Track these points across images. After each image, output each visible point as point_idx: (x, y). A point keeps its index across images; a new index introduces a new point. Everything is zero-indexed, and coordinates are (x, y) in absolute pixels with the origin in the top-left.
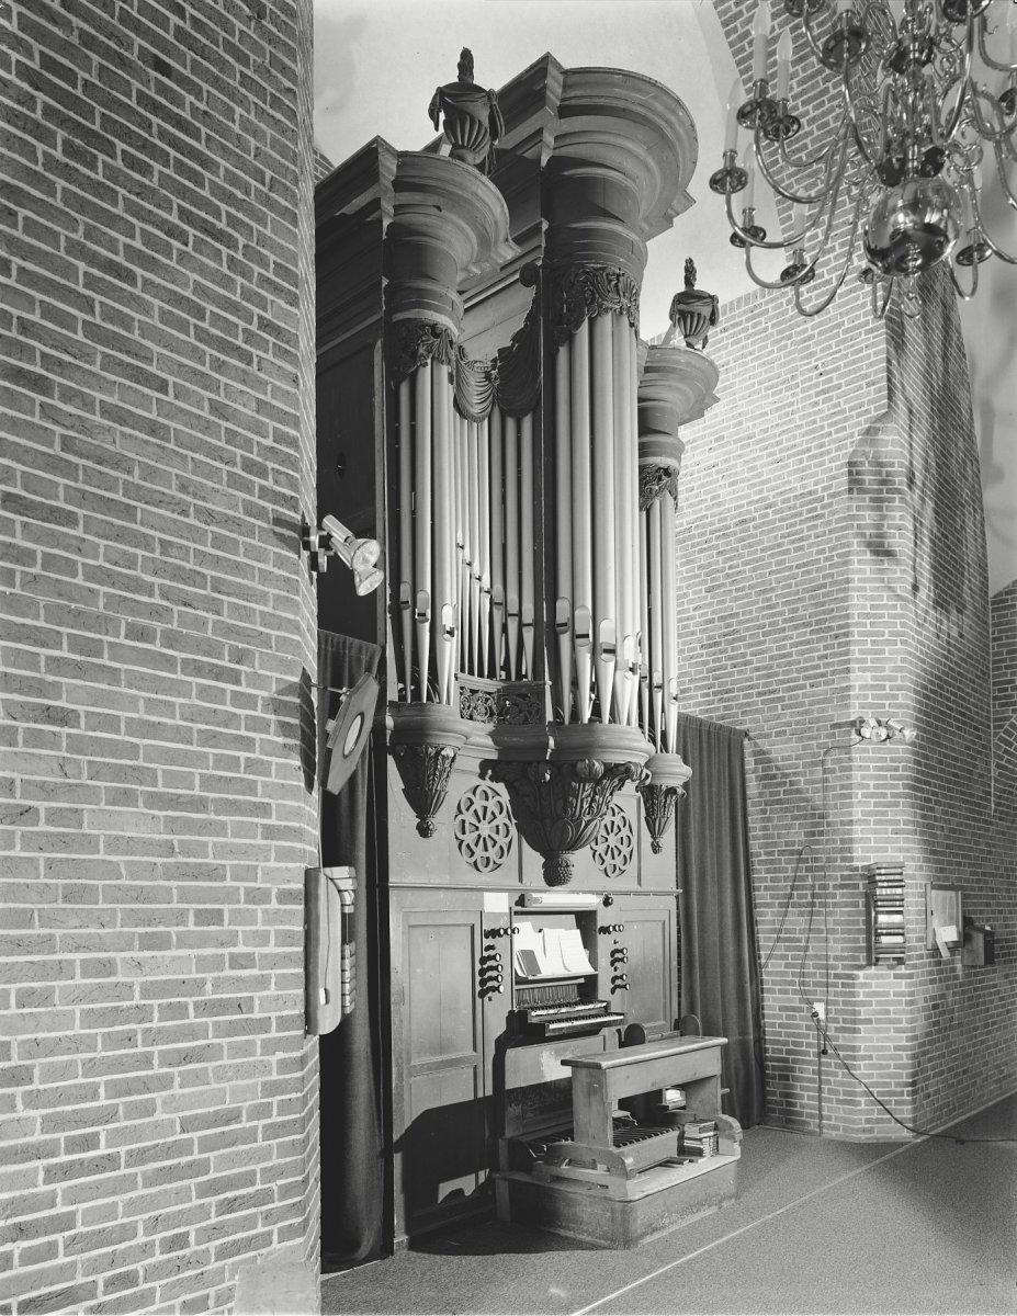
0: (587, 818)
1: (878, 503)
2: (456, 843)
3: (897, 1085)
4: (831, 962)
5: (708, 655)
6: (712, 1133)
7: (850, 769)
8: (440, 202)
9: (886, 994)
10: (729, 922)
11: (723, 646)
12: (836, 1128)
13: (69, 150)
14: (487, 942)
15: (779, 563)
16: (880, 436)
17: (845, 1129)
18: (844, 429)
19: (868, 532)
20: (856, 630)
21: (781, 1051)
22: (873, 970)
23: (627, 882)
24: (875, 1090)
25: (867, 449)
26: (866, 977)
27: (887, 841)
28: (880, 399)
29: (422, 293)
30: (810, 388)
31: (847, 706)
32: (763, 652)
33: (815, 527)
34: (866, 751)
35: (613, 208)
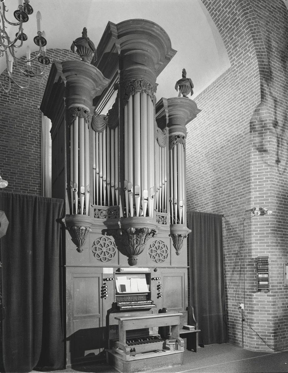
0: (137, 245)
1: (261, 134)
2: (93, 254)
3: (268, 333)
4: (246, 290)
5: (213, 191)
6: (174, 343)
7: (251, 225)
8: (76, 73)
10: (214, 277)
11: (217, 188)
12: (247, 346)
14: (104, 282)
15: (231, 159)
16: (261, 112)
17: (250, 346)
18: (249, 111)
19: (257, 145)
20: (253, 178)
21: (232, 319)
22: (259, 293)
23: (166, 264)
24: (260, 334)
25: (257, 117)
26: (256, 295)
27: (264, 249)
28: (259, 99)
29: (74, 99)
30: (239, 100)
31: (250, 204)
32: (227, 189)
33: (241, 145)
34: (257, 219)
35: (139, 61)
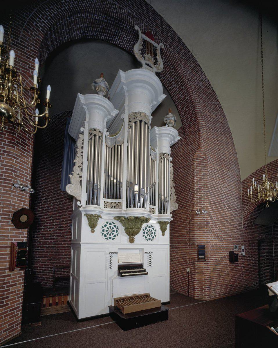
9: (202, 267)
13: (170, 34)
